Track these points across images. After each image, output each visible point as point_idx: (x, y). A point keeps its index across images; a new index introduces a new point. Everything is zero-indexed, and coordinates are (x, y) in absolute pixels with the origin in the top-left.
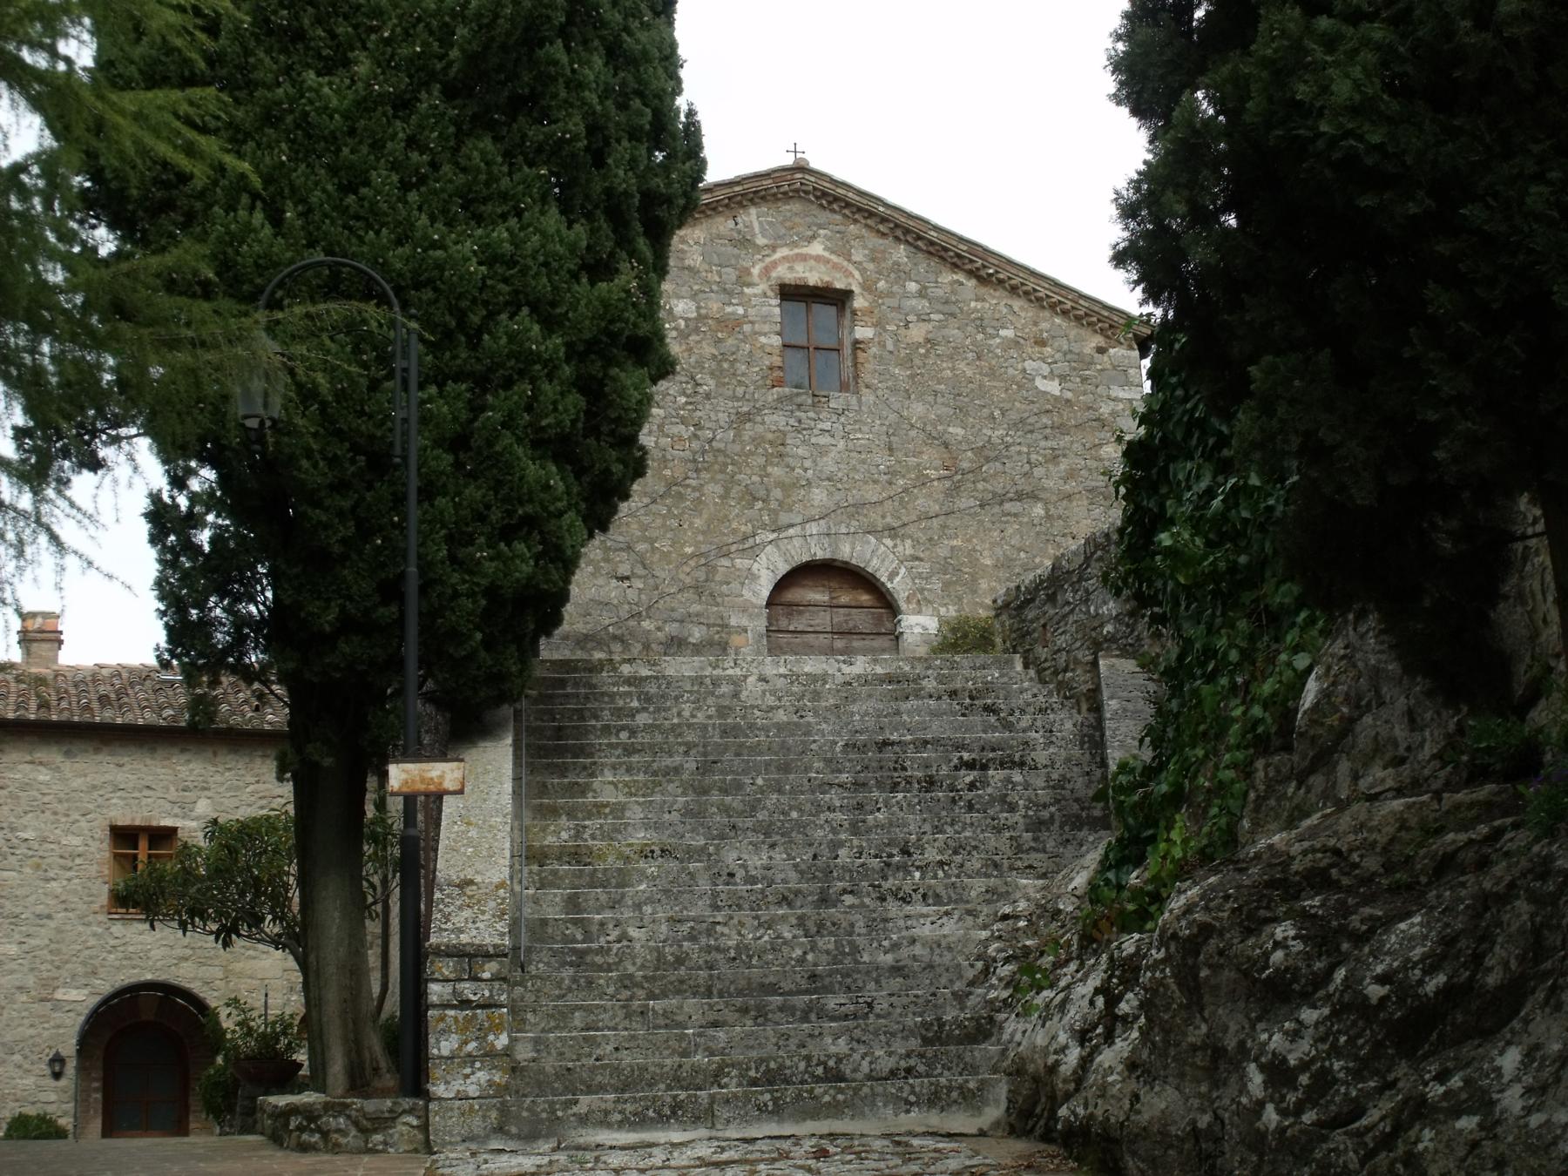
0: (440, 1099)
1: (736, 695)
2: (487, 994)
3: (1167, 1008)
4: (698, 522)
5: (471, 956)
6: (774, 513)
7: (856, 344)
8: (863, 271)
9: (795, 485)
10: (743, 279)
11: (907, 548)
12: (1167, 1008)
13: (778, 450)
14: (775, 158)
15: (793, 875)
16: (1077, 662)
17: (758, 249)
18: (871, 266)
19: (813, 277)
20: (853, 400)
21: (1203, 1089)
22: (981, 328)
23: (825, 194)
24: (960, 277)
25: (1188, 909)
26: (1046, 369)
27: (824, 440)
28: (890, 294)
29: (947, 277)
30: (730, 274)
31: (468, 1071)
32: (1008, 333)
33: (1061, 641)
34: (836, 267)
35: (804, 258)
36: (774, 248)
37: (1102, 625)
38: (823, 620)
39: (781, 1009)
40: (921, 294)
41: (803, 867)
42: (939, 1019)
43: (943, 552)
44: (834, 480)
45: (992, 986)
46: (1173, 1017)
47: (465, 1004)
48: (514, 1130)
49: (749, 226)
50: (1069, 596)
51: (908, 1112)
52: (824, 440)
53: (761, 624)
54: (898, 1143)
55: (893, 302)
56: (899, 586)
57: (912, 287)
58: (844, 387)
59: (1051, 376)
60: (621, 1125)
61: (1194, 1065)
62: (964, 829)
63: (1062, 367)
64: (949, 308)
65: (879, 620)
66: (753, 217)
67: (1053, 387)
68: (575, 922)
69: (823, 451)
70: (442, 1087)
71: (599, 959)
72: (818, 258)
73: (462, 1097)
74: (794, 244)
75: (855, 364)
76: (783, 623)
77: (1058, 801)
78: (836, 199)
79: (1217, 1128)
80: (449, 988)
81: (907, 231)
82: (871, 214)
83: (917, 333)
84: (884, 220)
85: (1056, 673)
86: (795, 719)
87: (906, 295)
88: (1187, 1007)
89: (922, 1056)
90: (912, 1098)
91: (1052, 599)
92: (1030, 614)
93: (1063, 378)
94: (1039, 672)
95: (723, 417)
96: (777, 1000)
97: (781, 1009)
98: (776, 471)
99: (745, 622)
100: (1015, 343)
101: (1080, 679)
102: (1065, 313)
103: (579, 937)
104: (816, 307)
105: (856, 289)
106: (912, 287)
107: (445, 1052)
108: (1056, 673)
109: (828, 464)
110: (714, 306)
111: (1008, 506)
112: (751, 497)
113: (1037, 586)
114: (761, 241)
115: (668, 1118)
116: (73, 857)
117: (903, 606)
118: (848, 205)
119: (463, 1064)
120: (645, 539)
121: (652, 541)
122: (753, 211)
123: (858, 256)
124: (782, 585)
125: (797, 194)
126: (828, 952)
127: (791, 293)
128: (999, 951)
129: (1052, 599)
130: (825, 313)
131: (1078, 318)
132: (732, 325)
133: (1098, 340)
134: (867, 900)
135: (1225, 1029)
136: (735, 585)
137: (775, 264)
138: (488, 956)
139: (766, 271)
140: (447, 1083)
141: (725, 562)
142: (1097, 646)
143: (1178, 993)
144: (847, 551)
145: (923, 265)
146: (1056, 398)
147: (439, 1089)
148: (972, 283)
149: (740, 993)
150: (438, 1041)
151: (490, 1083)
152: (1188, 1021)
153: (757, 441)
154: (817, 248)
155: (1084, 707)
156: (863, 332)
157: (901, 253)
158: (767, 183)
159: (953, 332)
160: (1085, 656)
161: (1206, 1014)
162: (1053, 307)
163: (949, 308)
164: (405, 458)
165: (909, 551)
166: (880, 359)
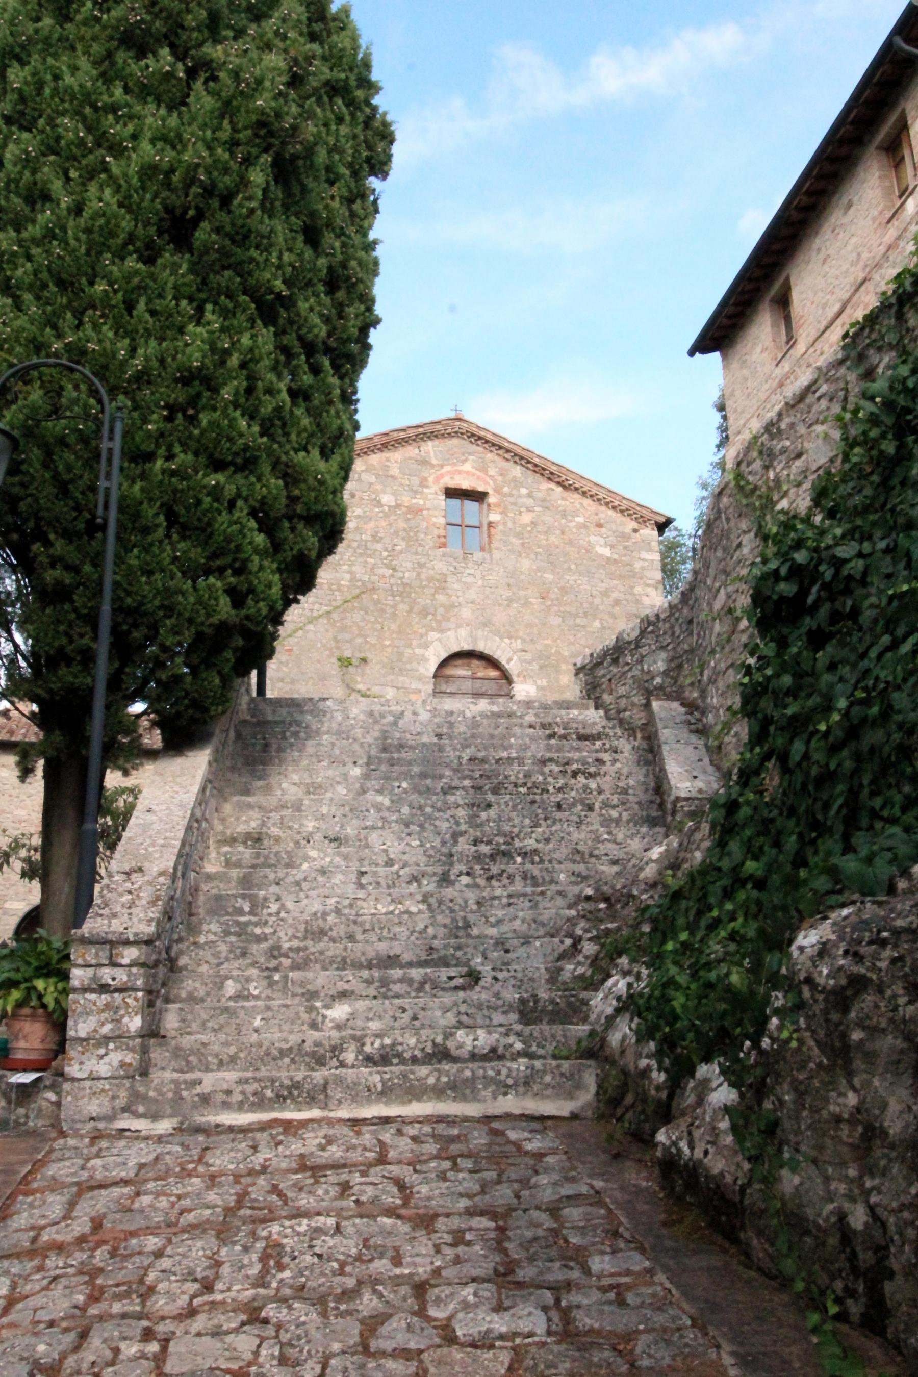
0: (74, 1080)
1: (395, 723)
2: (125, 978)
3: (802, 1067)
4: (394, 627)
5: (112, 944)
6: (439, 622)
7: (490, 525)
8: (494, 481)
9: (453, 606)
10: (423, 483)
11: (518, 644)
12: (802, 1067)
13: (441, 584)
14: (444, 413)
15: (423, 859)
16: (633, 704)
17: (432, 466)
18: (500, 478)
19: (465, 484)
20: (487, 556)
21: (852, 1172)
22: (564, 516)
23: (473, 435)
24: (553, 485)
25: (823, 950)
26: (602, 541)
27: (470, 580)
28: (511, 495)
29: (545, 485)
30: (415, 481)
31: (102, 1051)
32: (580, 519)
33: (622, 690)
34: (478, 478)
35: (460, 472)
36: (442, 466)
37: (653, 678)
38: (467, 685)
39: (401, 981)
40: (530, 495)
41: (432, 852)
42: (535, 996)
43: (539, 647)
44: (477, 605)
45: (579, 963)
46: (811, 1078)
47: (104, 988)
48: (141, 1109)
49: (427, 453)
50: (629, 659)
51: (505, 1094)
52: (470, 580)
53: (430, 688)
54: (495, 1132)
55: (512, 500)
56: (512, 667)
57: (524, 491)
58: (482, 549)
59: (606, 545)
60: (240, 1107)
61: (837, 1140)
62: (554, 823)
63: (612, 539)
64: (546, 505)
65: (501, 687)
66: (430, 448)
67: (607, 552)
68: (244, 897)
69: (468, 586)
70: (77, 1067)
71: (258, 931)
72: (468, 473)
73: (93, 1078)
74: (454, 464)
75: (489, 536)
76: (443, 687)
77: (624, 804)
78: (480, 438)
79: (877, 1233)
80: (90, 972)
81: (522, 458)
82: (500, 448)
83: (526, 518)
84: (508, 451)
85: (619, 712)
86: (435, 740)
87: (520, 496)
88: (830, 1069)
89: (518, 1034)
90: (510, 1081)
91: (615, 661)
92: (601, 672)
93: (612, 547)
94: (606, 713)
95: (409, 565)
96: (397, 973)
97: (401, 981)
98: (441, 598)
99: (420, 686)
100: (584, 526)
101: (637, 717)
102: (614, 508)
103: (247, 909)
104: (467, 502)
105: (490, 491)
106: (524, 491)
107: (82, 1034)
108: (619, 712)
109: (472, 594)
110: (406, 500)
111: (578, 621)
112: (424, 613)
113: (605, 653)
114: (434, 461)
115: (285, 1099)
116: (20, 822)
117: (515, 678)
118: (487, 442)
119: (98, 1045)
120: (360, 635)
121: (365, 637)
122: (430, 443)
123: (492, 472)
124: (444, 664)
125: (458, 434)
126: (445, 926)
127: (451, 493)
128: (586, 931)
129: (615, 661)
130: (471, 506)
131: (622, 511)
132: (416, 511)
133: (634, 525)
134: (478, 880)
135: (884, 1106)
136: (415, 665)
137: (442, 476)
138: (127, 943)
139: (437, 480)
140: (81, 1063)
141: (409, 651)
142: (648, 694)
143: (816, 1051)
144: (481, 647)
145: (531, 478)
146: (608, 559)
147: (73, 1070)
148: (560, 489)
149: (370, 966)
150: (76, 1023)
151: (123, 1065)
152: (831, 1085)
153: (430, 579)
154: (467, 467)
155: (639, 735)
156: (494, 517)
157: (517, 471)
158: (439, 427)
159: (548, 519)
160: (639, 700)
161: (856, 1081)
162: (607, 504)
163: (546, 505)
164: (106, 521)
165: (519, 646)
166: (504, 533)
